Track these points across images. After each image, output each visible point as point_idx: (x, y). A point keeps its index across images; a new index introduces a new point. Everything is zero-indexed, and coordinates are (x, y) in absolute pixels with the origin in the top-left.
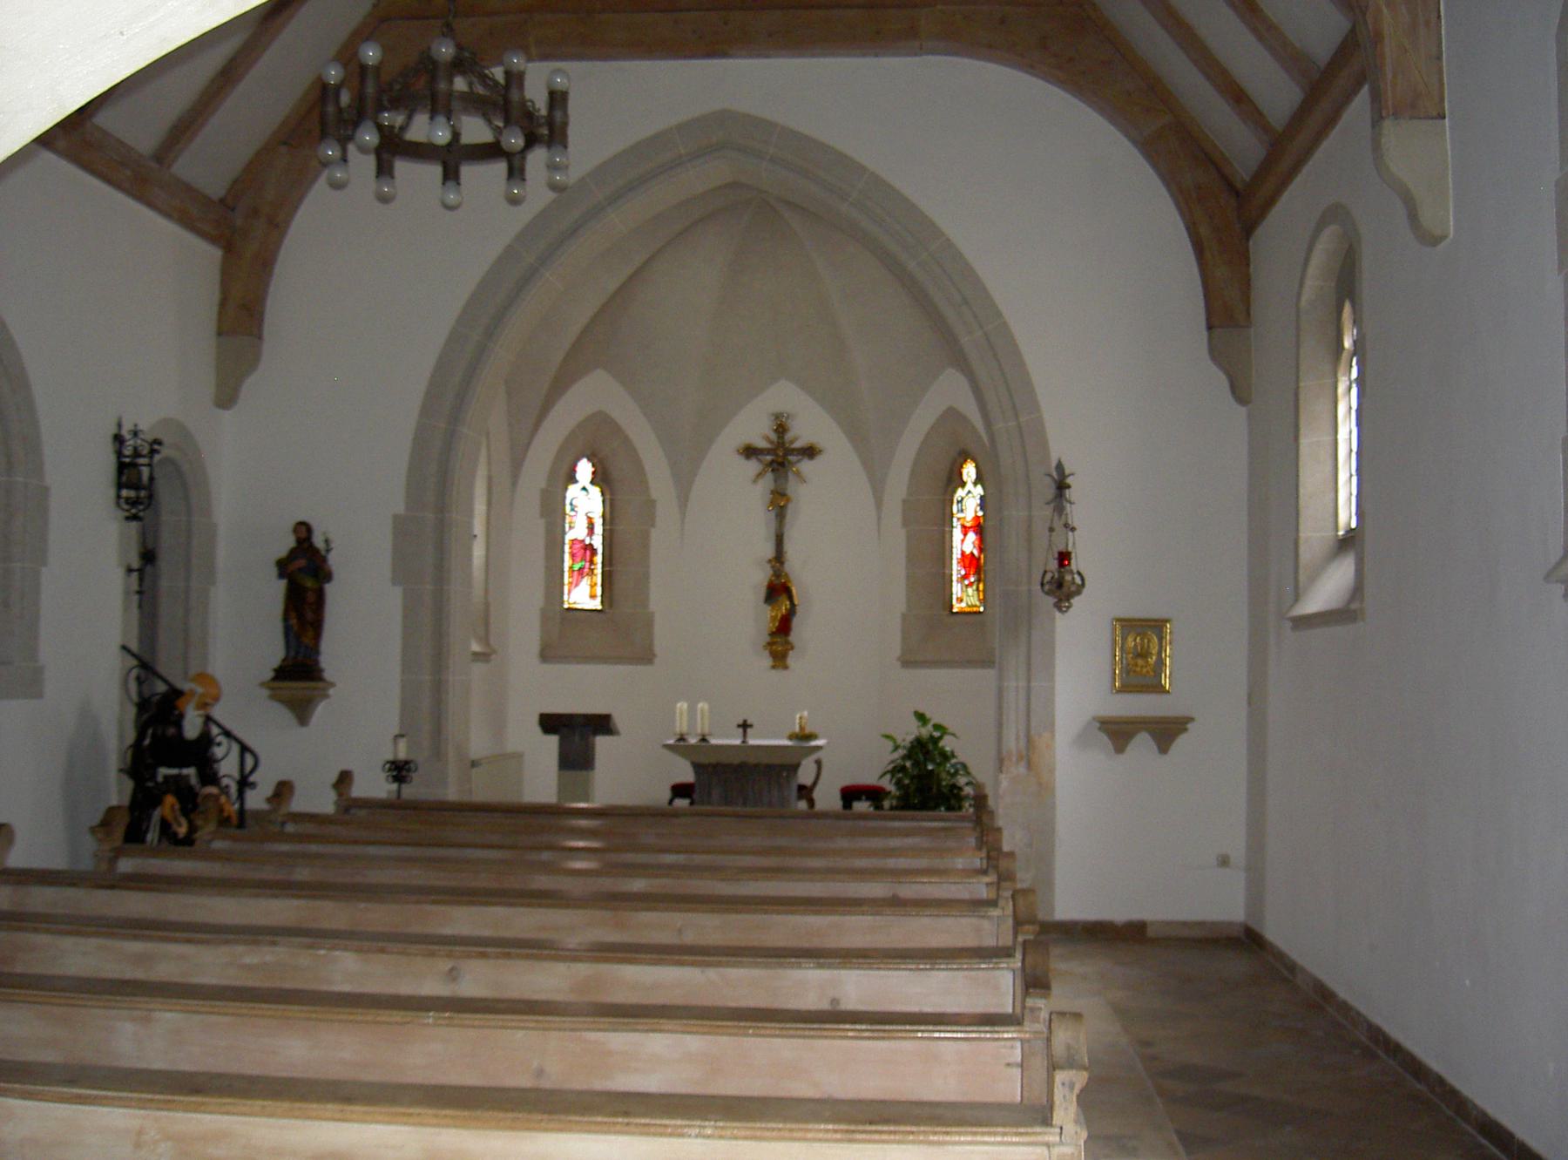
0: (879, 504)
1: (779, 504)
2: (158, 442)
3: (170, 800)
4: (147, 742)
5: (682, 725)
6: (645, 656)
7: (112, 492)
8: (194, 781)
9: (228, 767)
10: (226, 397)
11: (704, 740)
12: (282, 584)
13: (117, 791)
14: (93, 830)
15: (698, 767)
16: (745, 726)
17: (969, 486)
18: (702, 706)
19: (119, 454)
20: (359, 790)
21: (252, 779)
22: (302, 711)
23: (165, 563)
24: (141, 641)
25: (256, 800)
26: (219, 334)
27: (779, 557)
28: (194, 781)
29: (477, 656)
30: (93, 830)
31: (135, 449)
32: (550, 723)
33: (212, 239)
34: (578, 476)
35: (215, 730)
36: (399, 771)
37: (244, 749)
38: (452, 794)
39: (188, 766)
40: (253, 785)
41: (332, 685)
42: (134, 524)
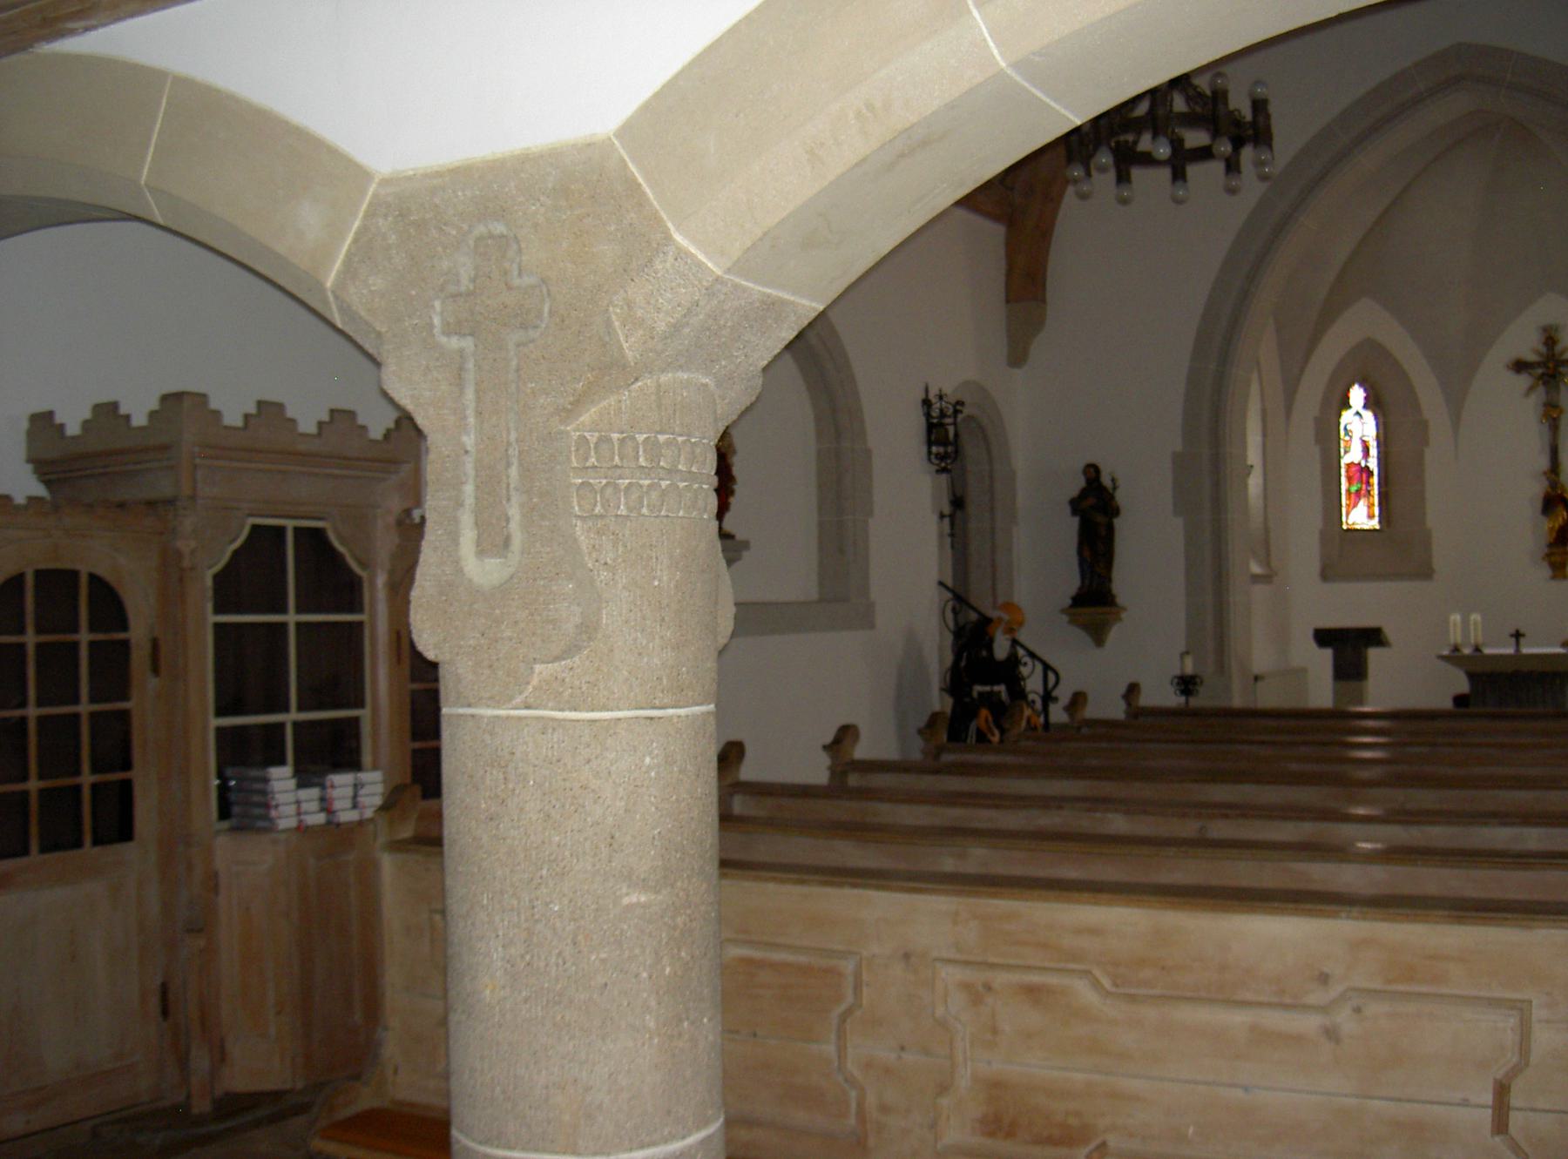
1: (1551, 415)
2: (960, 403)
3: (984, 713)
4: (963, 664)
5: (1456, 636)
6: (1425, 572)
7: (924, 449)
8: (1004, 696)
9: (1033, 684)
10: (1017, 356)
11: (1477, 649)
12: (1075, 522)
13: (939, 701)
14: (920, 732)
15: (1472, 676)
16: (1518, 635)
18: (1475, 617)
19: (928, 415)
20: (1146, 699)
21: (1054, 694)
22: (1098, 633)
23: (971, 508)
24: (955, 576)
25: (1058, 714)
26: (1008, 301)
28: (1004, 696)
29: (1256, 579)
30: (920, 732)
31: (941, 410)
32: (1324, 637)
33: (996, 218)
34: (1352, 402)
35: (1021, 652)
36: (1187, 684)
37: (1047, 667)
38: (1237, 702)
39: (998, 683)
40: (1056, 699)
41: (1125, 609)
42: (944, 477)
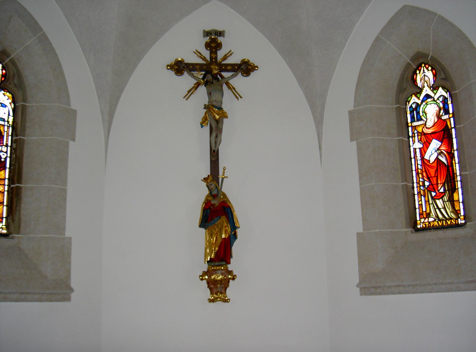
0: (319, 122)
1: (214, 120)
17: (427, 91)
27: (214, 177)
